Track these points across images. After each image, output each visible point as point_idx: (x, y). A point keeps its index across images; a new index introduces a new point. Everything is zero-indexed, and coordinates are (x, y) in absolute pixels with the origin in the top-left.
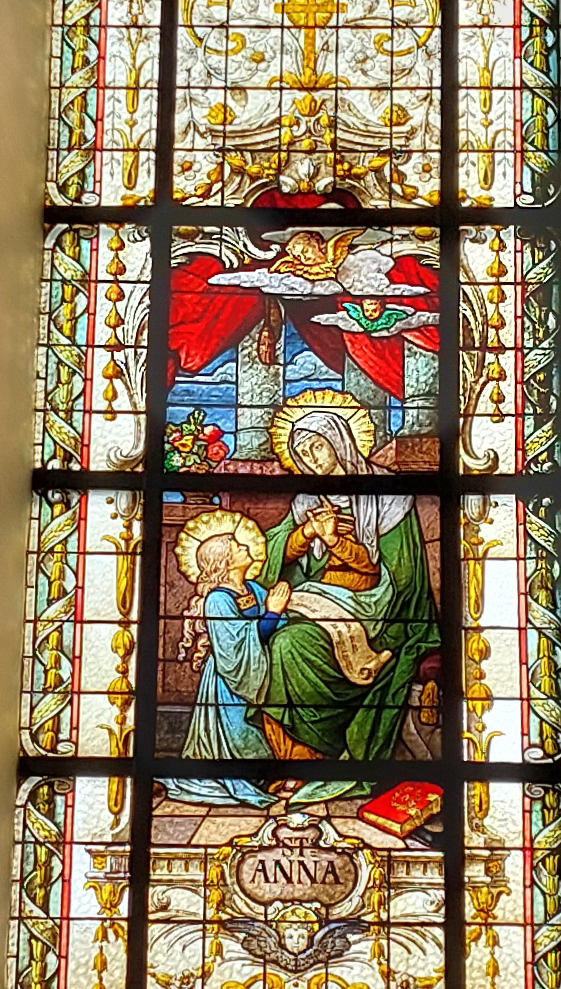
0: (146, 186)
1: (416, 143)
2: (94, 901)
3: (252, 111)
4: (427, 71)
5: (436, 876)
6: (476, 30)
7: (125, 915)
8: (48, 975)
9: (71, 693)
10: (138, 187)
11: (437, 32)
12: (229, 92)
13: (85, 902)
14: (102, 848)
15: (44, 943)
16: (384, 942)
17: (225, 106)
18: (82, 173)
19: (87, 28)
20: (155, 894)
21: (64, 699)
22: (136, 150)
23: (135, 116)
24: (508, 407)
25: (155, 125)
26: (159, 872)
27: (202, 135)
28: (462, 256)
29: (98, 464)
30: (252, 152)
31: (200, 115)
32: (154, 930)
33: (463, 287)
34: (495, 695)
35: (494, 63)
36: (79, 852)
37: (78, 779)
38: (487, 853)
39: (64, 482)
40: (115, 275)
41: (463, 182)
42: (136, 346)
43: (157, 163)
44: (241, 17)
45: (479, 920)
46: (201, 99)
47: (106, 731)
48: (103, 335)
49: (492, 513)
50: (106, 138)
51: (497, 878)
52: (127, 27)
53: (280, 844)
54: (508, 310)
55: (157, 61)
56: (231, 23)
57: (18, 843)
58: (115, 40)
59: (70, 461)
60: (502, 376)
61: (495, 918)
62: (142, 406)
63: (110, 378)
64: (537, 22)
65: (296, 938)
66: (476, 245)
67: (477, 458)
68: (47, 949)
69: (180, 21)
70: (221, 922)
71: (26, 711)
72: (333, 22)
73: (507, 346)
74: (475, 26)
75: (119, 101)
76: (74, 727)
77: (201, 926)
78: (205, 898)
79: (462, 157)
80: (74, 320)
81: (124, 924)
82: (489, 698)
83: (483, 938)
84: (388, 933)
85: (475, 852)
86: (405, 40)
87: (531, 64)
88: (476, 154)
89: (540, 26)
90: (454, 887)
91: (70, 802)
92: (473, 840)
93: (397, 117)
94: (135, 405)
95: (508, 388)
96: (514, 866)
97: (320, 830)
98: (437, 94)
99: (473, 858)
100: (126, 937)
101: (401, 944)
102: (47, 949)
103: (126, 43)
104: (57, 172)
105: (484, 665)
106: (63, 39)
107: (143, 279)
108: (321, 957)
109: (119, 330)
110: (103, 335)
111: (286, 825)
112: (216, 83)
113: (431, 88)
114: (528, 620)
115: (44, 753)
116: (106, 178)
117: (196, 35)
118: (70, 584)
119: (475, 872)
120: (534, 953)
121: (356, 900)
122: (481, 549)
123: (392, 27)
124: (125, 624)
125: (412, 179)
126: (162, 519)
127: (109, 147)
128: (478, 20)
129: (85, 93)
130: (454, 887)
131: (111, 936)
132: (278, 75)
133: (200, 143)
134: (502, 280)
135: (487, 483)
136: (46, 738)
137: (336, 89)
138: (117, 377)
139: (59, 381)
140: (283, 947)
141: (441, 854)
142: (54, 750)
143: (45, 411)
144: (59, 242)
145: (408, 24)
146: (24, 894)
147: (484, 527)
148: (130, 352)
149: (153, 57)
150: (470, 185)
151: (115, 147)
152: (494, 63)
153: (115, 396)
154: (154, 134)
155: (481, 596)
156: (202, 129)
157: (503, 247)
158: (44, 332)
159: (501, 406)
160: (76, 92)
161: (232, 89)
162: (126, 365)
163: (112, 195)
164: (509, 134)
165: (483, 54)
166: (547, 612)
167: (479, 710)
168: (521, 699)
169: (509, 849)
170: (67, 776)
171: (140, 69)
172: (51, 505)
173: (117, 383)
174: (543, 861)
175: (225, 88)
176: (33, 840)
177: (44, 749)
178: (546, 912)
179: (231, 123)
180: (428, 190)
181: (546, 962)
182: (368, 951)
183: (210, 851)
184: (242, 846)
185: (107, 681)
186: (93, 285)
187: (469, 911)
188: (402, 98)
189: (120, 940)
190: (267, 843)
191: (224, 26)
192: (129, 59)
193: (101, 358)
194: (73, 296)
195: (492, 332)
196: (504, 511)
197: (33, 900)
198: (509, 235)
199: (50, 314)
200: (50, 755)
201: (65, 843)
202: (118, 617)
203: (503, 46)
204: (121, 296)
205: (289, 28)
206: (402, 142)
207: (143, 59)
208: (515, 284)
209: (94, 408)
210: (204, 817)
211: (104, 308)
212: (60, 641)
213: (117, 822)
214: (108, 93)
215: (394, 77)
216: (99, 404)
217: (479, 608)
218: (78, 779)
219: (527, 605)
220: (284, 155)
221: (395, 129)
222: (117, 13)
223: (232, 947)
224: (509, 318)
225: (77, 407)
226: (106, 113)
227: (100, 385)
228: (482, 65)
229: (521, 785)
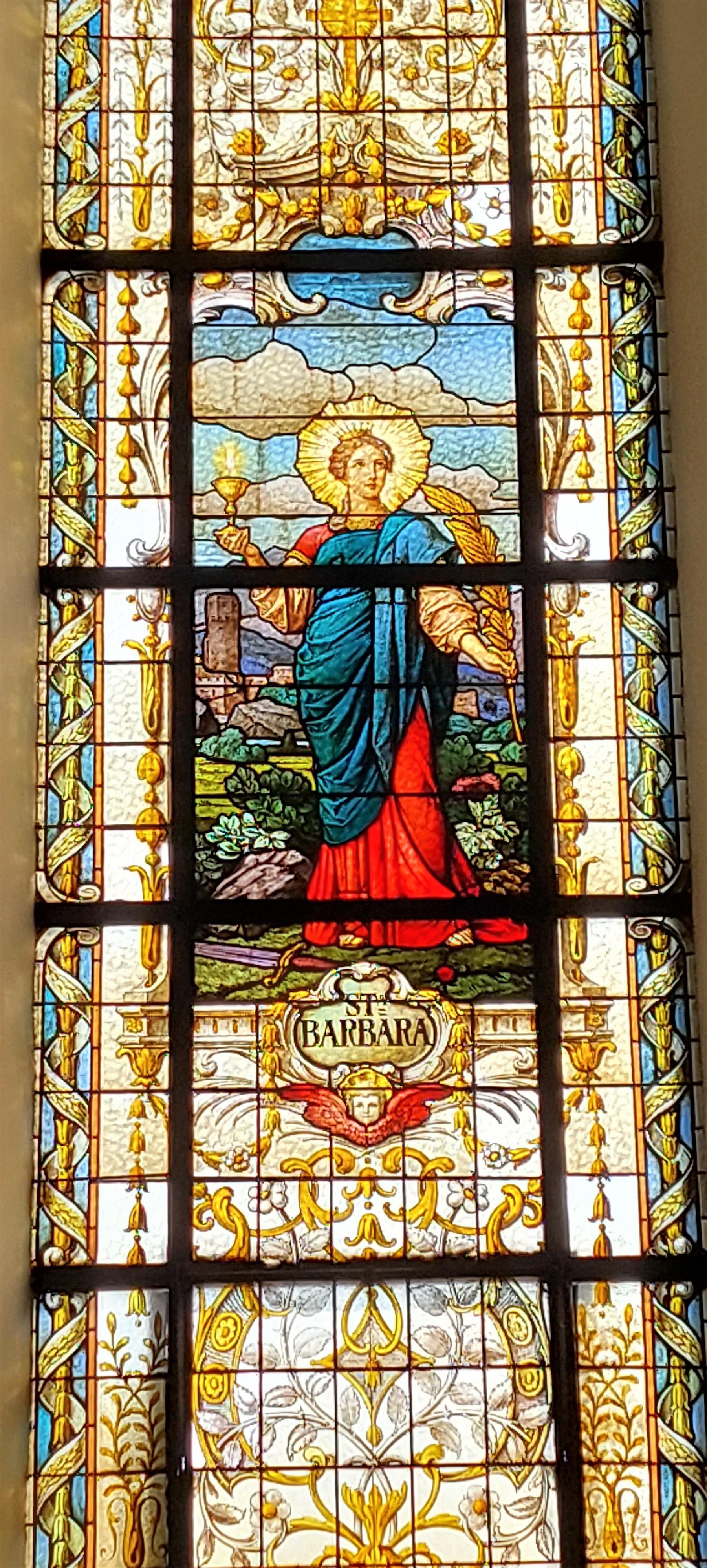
0: (160, 229)
1: (479, 174)
2: (128, 1069)
3: (285, 137)
4: (491, 86)
5: (526, 1031)
6: (546, 38)
7: (165, 1085)
8: (85, 383)
9: (93, 829)
10: (152, 228)
11: (501, 42)
12: (256, 115)
13: (116, 1070)
14: (137, 1009)
15: (70, 1121)
16: (469, 1110)
17: (253, 131)
18: (77, 858)
19: (69, 1379)
20: (200, 1058)
21: (85, 834)
22: (149, 185)
23: (146, 145)
24: (599, 481)
25: (170, 155)
26: (203, 1033)
27: (227, 167)
28: (538, 303)
29: (117, 557)
30: (287, 186)
31: (224, 144)
32: (199, 1101)
33: (542, 342)
34: (590, 817)
35: (568, 77)
36: (109, 1015)
37: (101, 1294)
38: (586, 1003)
39: (79, 263)
40: (128, 333)
41: (538, 219)
42: (156, 419)
43: (174, 200)
44: (267, 27)
45: (580, 1082)
46: (224, 124)
47: (136, 874)
48: (116, 406)
49: (583, 604)
50: (113, 171)
51: (600, 1042)
52: (134, 39)
53: (342, 998)
54: (595, 368)
55: (170, 79)
56: (255, 34)
57: (37, 1004)
58: (120, 53)
59: (82, 556)
60: (589, 447)
61: (598, 1078)
62: (165, 490)
63: (128, 457)
64: (618, 28)
65: (366, 1106)
66: (555, 291)
67: (565, 545)
68: (81, 452)
69: (196, 32)
70: (277, 1090)
71: (52, 16)
72: (377, 32)
73: (594, 410)
74: (545, 34)
75: (126, 127)
76: (98, 869)
77: (254, 1095)
78: (258, 1061)
79: (536, 187)
80: (74, 1059)
81: (165, 1098)
82: (583, 820)
83: (585, 1101)
84: (474, 1098)
85: (572, 1003)
86: (463, 55)
87: (613, 77)
88: (550, 184)
89: (621, 32)
90: (548, 1042)
91: (96, 957)
92: (566, 987)
93: (457, 141)
94: (154, 482)
95: (598, 459)
96: (619, 1019)
97: (390, 981)
98: (503, 116)
99: (573, 1011)
100: (167, 1111)
101: (490, 1112)
102: (74, 1128)
103: (134, 60)
104: (46, 858)
105: (579, 783)
106: (58, 53)
107: (160, 340)
108: (396, 1128)
109: (135, 401)
110: (116, 406)
111: (350, 976)
112: (241, 105)
113: (496, 110)
114: (627, 728)
115: (64, 897)
116: (113, 220)
117: (215, 48)
118: (78, 1419)
119: (571, 1025)
120: (644, 1119)
121: (434, 1059)
122: (571, 645)
123: (447, 38)
124: (154, 745)
125: (479, 216)
126: (193, 787)
127: (116, 181)
128: (548, 26)
129: (80, 750)
130: (548, 1042)
131: (149, 1109)
132: (315, 95)
133: (227, 176)
134: (586, 332)
135: (577, 572)
136: (65, 881)
137: (383, 111)
138: (134, 456)
139: (59, 1030)
140: (352, 1118)
141: (533, 1006)
142: (74, 894)
143: (50, 498)
144: (59, 295)
145: (465, 36)
146: (56, 396)
147: (573, 619)
148: (150, 425)
149: (164, 75)
150: (545, 222)
151: (124, 181)
152: (568, 77)
153: (133, 477)
154: (169, 165)
155: (573, 698)
156: (226, 160)
157: (586, 295)
158: (47, 402)
159: (590, 480)
160: (74, 117)
161: (260, 111)
162: (146, 444)
163: (121, 235)
164: (588, 160)
165: (555, 68)
166: (647, 717)
167: (571, 835)
168: (629, 998)
169: (611, 998)
170: (93, 925)
171: (150, 87)
172: (52, 1312)
173: (136, 462)
174: (652, 1010)
175: (252, 111)
176: (62, 339)
177: (63, 893)
178: (663, 1181)
179: (261, 152)
180: (498, 229)
181: (660, 1125)
182: (451, 1120)
183: (262, 1007)
184: (299, 1002)
185: (135, 812)
186: (101, 347)
187: (568, 1071)
188: (462, 121)
189: (160, 1115)
190: (329, 997)
191: (249, 37)
192: (136, 77)
193: (115, 434)
194: (72, 1025)
195: (576, 396)
196: (607, 936)
197: (57, 1071)
198: (592, 279)
199: (44, 1049)
200: (70, 900)
201: (98, 342)
202: (147, 738)
203: (579, 60)
204: (134, 361)
205: (324, 39)
206: (463, 172)
207: (152, 167)
208: (601, 337)
209: (106, 740)
210: (254, 230)
211: (116, 376)
212: (78, 767)
213: (154, 978)
214: (113, 117)
215: (452, 98)
216: (115, 486)
217: (572, 712)
218: (101, 1294)
219: (600, 79)
220: (325, 190)
221: (455, 159)
222: (121, 23)
223: (291, 1115)
224: (597, 379)
225: (88, 497)
226: (112, 142)
227: (115, 466)
228: (555, 80)
229: (623, 920)
